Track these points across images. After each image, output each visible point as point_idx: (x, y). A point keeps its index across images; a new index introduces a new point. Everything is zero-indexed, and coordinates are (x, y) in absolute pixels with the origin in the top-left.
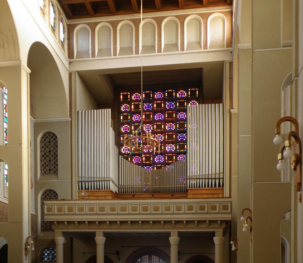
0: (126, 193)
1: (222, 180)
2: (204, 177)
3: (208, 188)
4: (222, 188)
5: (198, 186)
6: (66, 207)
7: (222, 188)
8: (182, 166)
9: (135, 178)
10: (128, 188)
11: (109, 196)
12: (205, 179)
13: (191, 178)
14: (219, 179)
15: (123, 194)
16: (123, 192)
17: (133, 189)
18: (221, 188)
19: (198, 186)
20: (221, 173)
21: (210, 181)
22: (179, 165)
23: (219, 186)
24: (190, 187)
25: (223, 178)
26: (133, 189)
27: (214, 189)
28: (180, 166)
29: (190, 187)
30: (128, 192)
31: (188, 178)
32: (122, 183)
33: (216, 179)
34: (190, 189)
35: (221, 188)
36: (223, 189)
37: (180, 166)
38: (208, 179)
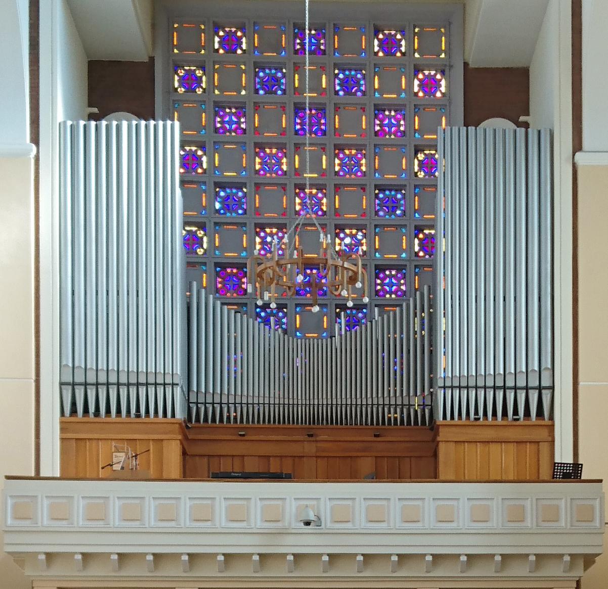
0: (214, 420)
1: (549, 396)
2: (490, 383)
3: (505, 423)
4: (550, 423)
5: (92, 409)
6: (563, 524)
7: (550, 423)
8: (402, 339)
9: (398, 368)
10: (241, 404)
11: (546, 443)
12: (118, 384)
13: (448, 384)
14: (540, 389)
15: (204, 427)
16: (206, 420)
17: (251, 407)
18: (547, 421)
19: (92, 409)
20: (102, 370)
21: (123, 391)
22: (391, 336)
23: (540, 413)
24: (445, 417)
25: (552, 388)
26: (251, 407)
27: (482, 425)
28: (395, 339)
29: (445, 417)
30: (221, 420)
31: (440, 383)
32: (202, 385)
33: (518, 391)
34: (445, 422)
35: (547, 421)
36: (553, 425)
37: (395, 339)
38: (495, 388)
